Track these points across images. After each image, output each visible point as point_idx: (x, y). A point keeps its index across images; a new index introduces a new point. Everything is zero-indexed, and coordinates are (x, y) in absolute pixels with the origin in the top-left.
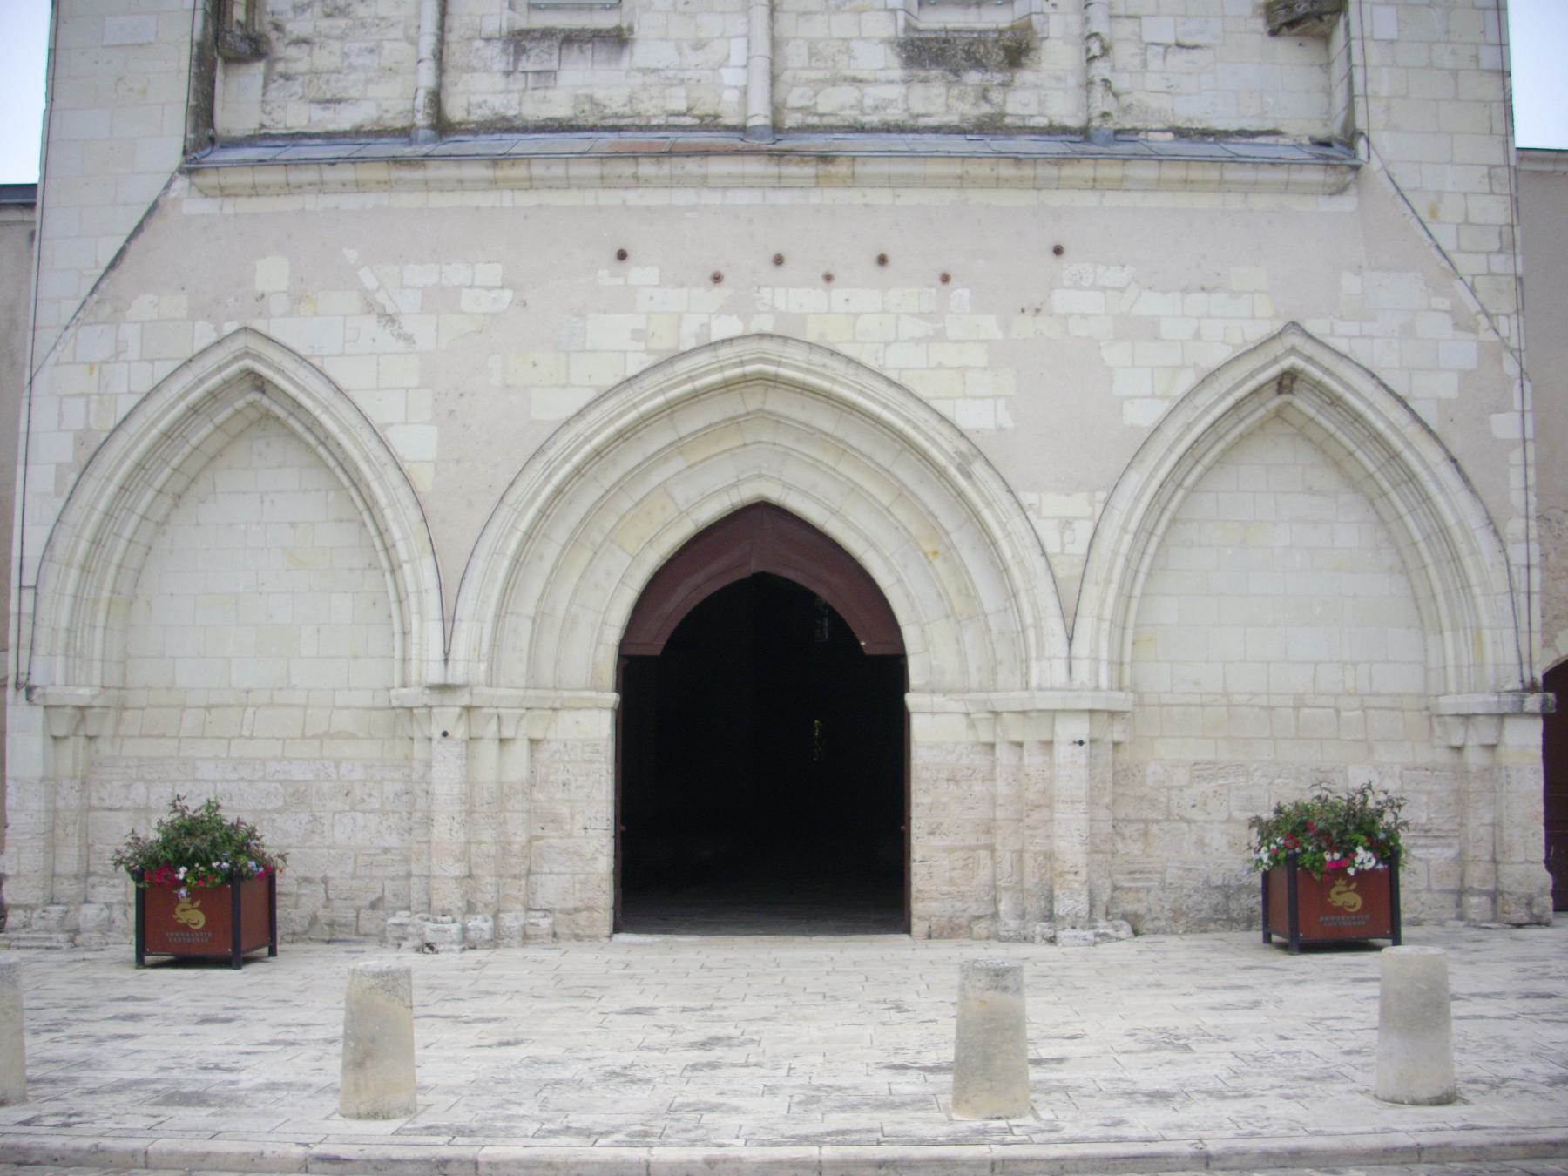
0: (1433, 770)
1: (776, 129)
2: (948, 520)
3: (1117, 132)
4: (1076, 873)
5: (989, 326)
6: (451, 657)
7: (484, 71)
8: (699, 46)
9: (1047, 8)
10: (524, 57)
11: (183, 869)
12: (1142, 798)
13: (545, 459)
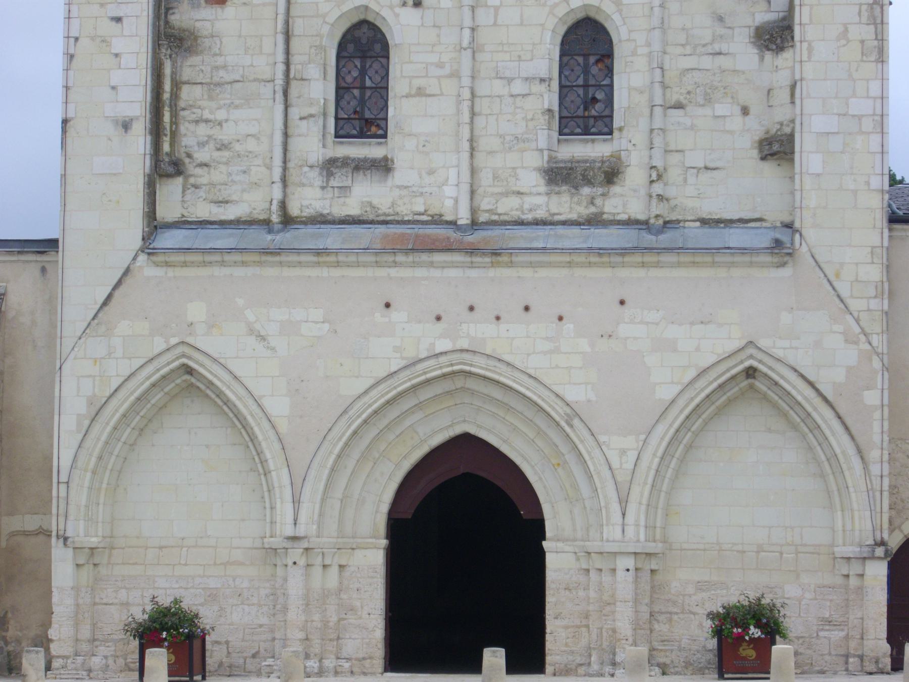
0: (834, 588)
1: (475, 224)
2: (564, 448)
3: (666, 223)
4: (627, 640)
5: (584, 345)
6: (298, 522)
7: (309, 186)
8: (431, 172)
9: (630, 147)
10: (332, 178)
11: (165, 633)
12: (668, 600)
13: (347, 416)
